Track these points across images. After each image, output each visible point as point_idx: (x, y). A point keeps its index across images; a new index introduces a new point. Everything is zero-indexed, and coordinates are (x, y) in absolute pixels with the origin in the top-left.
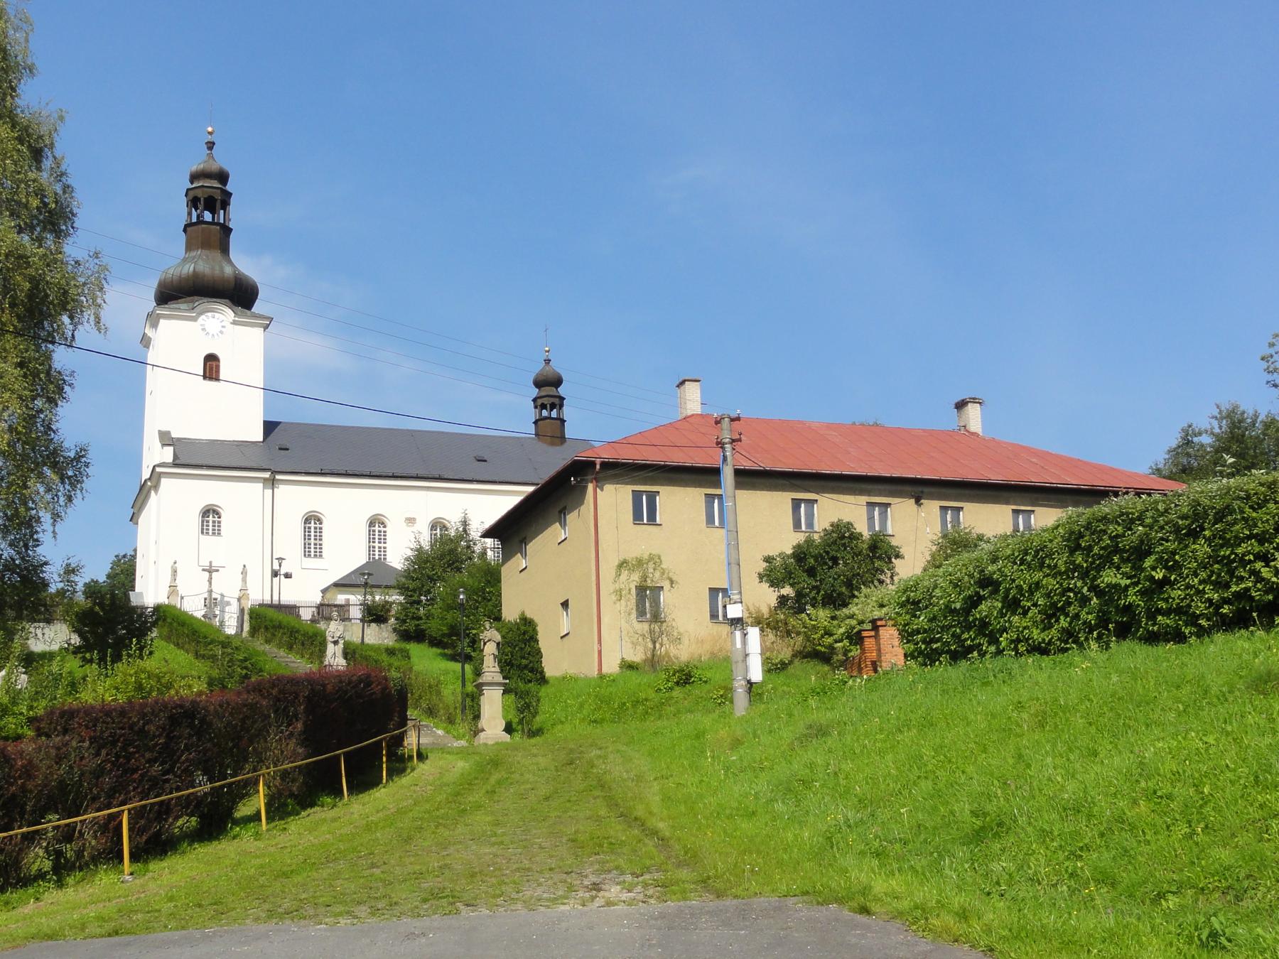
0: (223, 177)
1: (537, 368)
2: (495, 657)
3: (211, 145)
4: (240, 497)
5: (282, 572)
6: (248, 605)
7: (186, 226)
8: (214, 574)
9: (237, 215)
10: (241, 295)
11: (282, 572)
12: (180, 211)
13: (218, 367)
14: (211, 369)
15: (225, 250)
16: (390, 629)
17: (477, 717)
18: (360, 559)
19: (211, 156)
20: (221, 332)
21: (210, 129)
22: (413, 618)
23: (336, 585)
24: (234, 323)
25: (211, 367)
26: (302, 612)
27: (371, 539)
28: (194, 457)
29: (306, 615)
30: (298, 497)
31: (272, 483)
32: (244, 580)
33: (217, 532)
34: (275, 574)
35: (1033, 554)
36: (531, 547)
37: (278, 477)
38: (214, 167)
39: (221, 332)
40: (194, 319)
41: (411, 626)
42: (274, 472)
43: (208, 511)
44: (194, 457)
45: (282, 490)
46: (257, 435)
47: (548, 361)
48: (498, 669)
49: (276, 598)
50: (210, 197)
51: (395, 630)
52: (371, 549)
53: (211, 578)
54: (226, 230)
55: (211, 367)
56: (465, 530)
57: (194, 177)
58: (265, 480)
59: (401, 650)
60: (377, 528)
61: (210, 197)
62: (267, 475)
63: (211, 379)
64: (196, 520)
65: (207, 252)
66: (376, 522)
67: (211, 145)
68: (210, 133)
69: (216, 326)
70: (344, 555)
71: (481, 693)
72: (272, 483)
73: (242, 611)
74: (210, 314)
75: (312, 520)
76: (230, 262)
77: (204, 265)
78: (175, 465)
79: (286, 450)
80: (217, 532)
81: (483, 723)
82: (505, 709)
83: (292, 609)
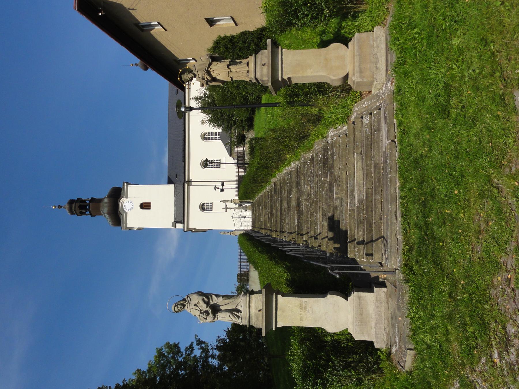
0: (71, 202)
2: (233, 63)
3: (60, 207)
4: (196, 195)
5: (221, 187)
7: (92, 216)
9: (86, 196)
10: (117, 194)
11: (221, 187)
12: (86, 218)
13: (146, 203)
15: (100, 200)
16: (247, 133)
17: (321, 88)
19: (64, 207)
22: (242, 123)
24: (127, 197)
25: (145, 206)
26: (241, 174)
27: (212, 139)
28: (181, 215)
29: (242, 173)
30: (195, 171)
31: (189, 182)
33: (211, 204)
34: (222, 190)
36: (180, 57)
37: (187, 179)
38: (67, 206)
40: (126, 213)
41: (245, 124)
42: (185, 182)
43: (202, 208)
44: (181, 215)
45: (192, 178)
46: (172, 186)
48: (251, 59)
49: (235, 186)
50: (81, 207)
51: (248, 131)
52: (216, 139)
54: (93, 200)
55: (145, 206)
56: (200, 99)
57: (72, 213)
58: (188, 185)
59: (250, 143)
60: (207, 137)
61: (81, 207)
62: (186, 185)
63: (150, 206)
65: (101, 209)
66: (204, 137)
67: (60, 207)
68: (55, 207)
69: (130, 203)
70: (218, 150)
71: (286, 83)
72: (189, 182)
74: (124, 207)
75: (206, 164)
76: (104, 198)
77: (105, 209)
79: (177, 176)
80: (211, 204)
81: (334, 78)
82: (302, 44)
83: (240, 180)
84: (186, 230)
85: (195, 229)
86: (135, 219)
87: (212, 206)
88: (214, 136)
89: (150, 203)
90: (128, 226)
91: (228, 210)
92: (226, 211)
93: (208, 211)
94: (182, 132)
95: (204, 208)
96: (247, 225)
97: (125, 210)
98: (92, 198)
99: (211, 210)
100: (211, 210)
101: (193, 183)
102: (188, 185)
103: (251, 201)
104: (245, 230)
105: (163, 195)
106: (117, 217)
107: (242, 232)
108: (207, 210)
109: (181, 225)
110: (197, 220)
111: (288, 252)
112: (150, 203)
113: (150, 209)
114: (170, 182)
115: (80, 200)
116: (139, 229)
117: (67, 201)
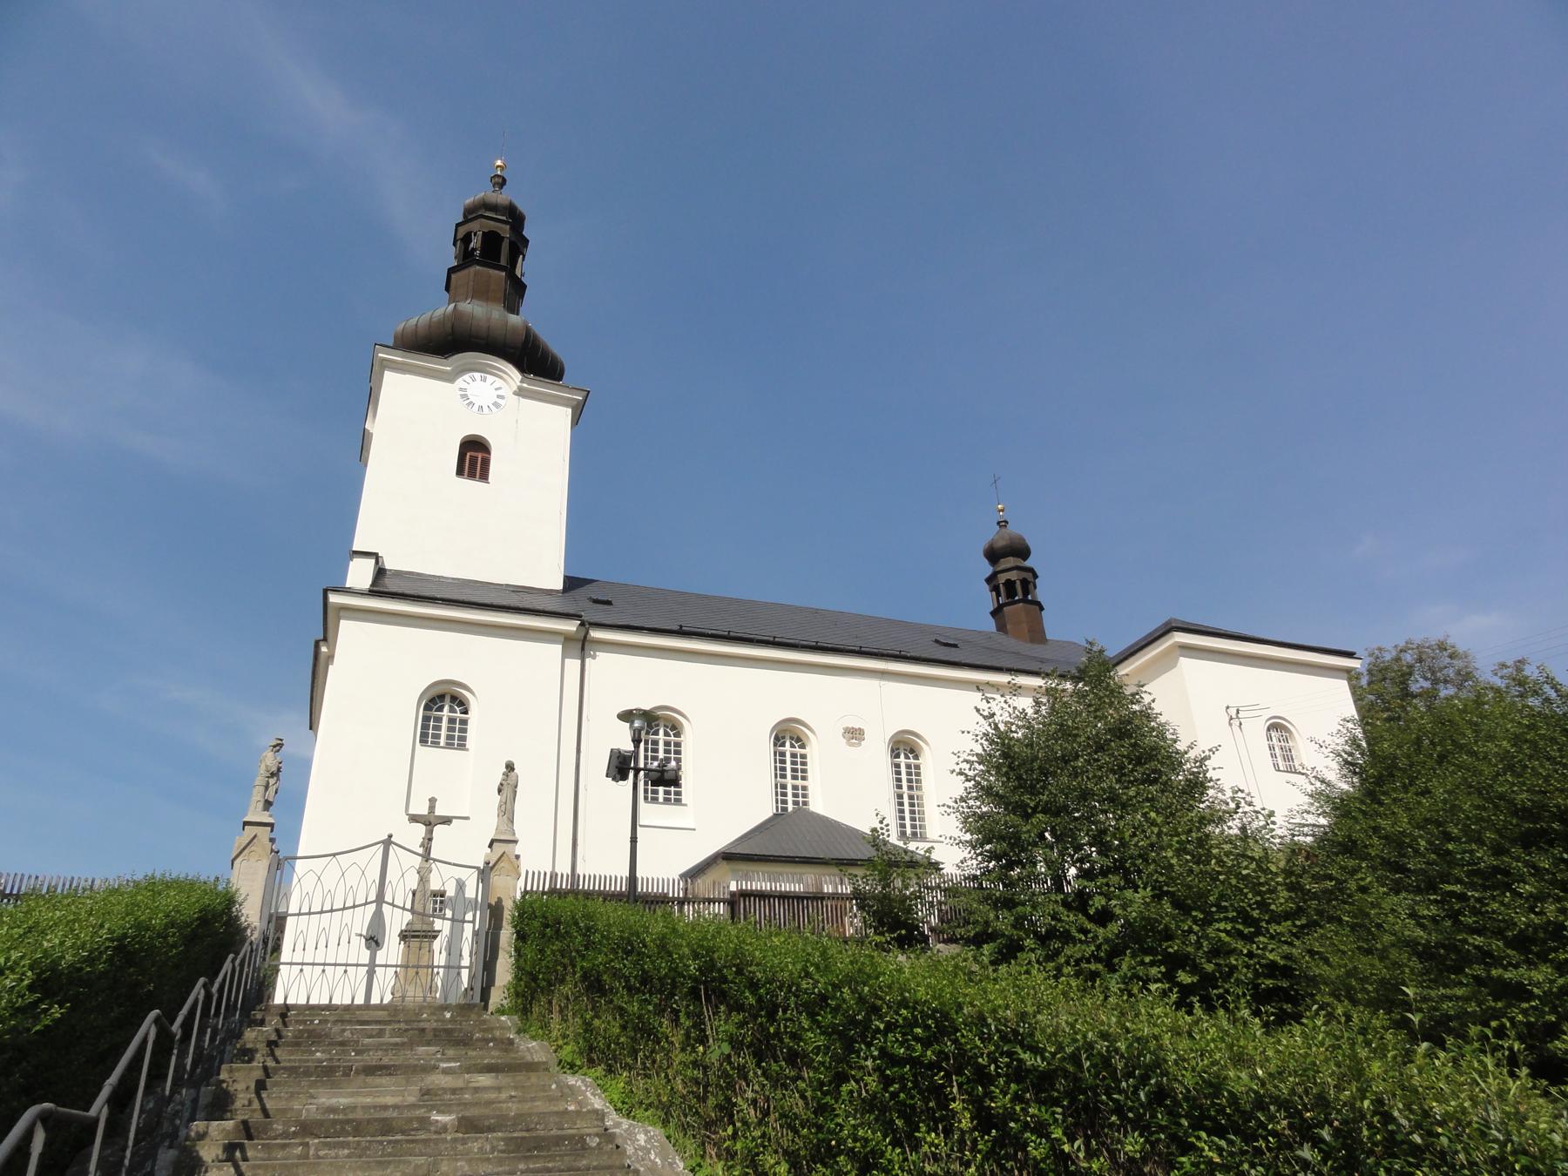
0: (515, 218)
1: (989, 534)
4: (513, 676)
6: (511, 890)
8: (439, 830)
10: (536, 362)
14: (473, 461)
18: (763, 809)
20: (496, 405)
21: (499, 163)
23: (727, 857)
24: (520, 393)
25: (474, 457)
30: (630, 676)
31: (580, 646)
32: (507, 812)
35: (1035, 1068)
37: (596, 634)
38: (503, 197)
39: (496, 405)
40: (450, 378)
43: (442, 697)
45: (601, 663)
46: (559, 586)
47: (1003, 524)
50: (493, 243)
53: (429, 839)
55: (474, 457)
61: (493, 243)
62: (571, 626)
63: (472, 476)
64: (408, 714)
69: (489, 396)
72: (580, 646)
73: (495, 911)
74: (477, 375)
78: (374, 592)
80: (458, 741)
84: (334, 598)
85: (330, 658)
86: (420, 410)
87: (449, 746)
88: (789, 782)
89: (484, 477)
90: (389, 377)
91: (420, 829)
92: (414, 819)
93: (425, 727)
94: (812, 639)
95: (443, 708)
96: (322, 964)
97: (467, 377)
98: (524, 287)
99: (423, 741)
100: (423, 741)
101: (573, 665)
102: (566, 639)
103: (497, 997)
104: (272, 944)
105: (522, 528)
106: (445, 344)
107: (251, 914)
108: (426, 719)
109: (366, 583)
110: (377, 667)
111: (233, 961)
112: (484, 477)
113: (460, 472)
114: (571, 583)
115: (519, 245)
116: (365, 439)
117: (522, 206)
